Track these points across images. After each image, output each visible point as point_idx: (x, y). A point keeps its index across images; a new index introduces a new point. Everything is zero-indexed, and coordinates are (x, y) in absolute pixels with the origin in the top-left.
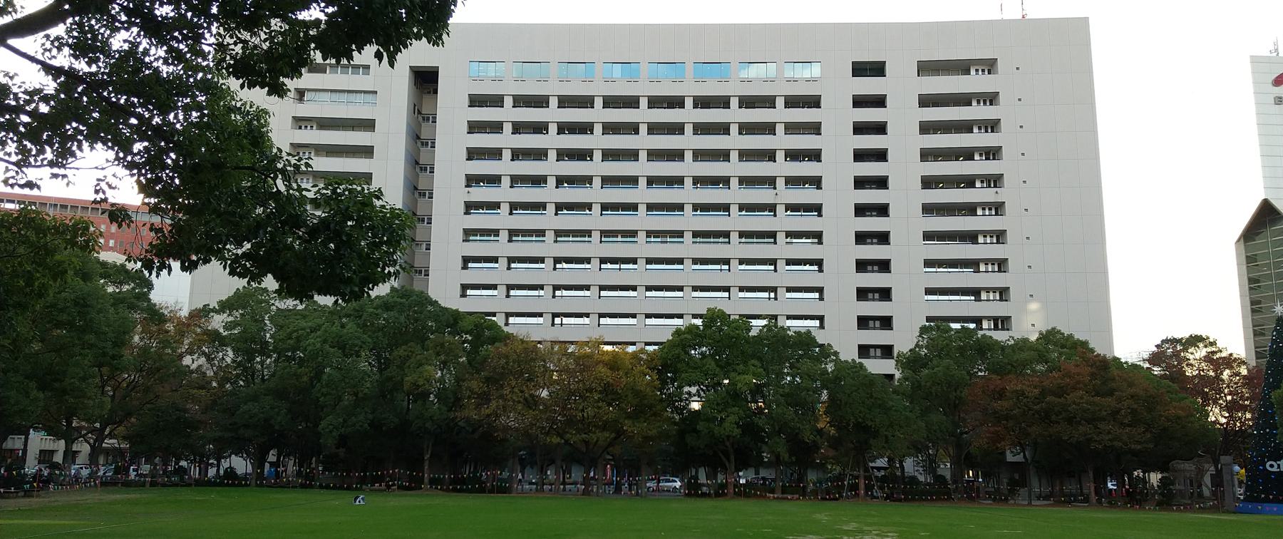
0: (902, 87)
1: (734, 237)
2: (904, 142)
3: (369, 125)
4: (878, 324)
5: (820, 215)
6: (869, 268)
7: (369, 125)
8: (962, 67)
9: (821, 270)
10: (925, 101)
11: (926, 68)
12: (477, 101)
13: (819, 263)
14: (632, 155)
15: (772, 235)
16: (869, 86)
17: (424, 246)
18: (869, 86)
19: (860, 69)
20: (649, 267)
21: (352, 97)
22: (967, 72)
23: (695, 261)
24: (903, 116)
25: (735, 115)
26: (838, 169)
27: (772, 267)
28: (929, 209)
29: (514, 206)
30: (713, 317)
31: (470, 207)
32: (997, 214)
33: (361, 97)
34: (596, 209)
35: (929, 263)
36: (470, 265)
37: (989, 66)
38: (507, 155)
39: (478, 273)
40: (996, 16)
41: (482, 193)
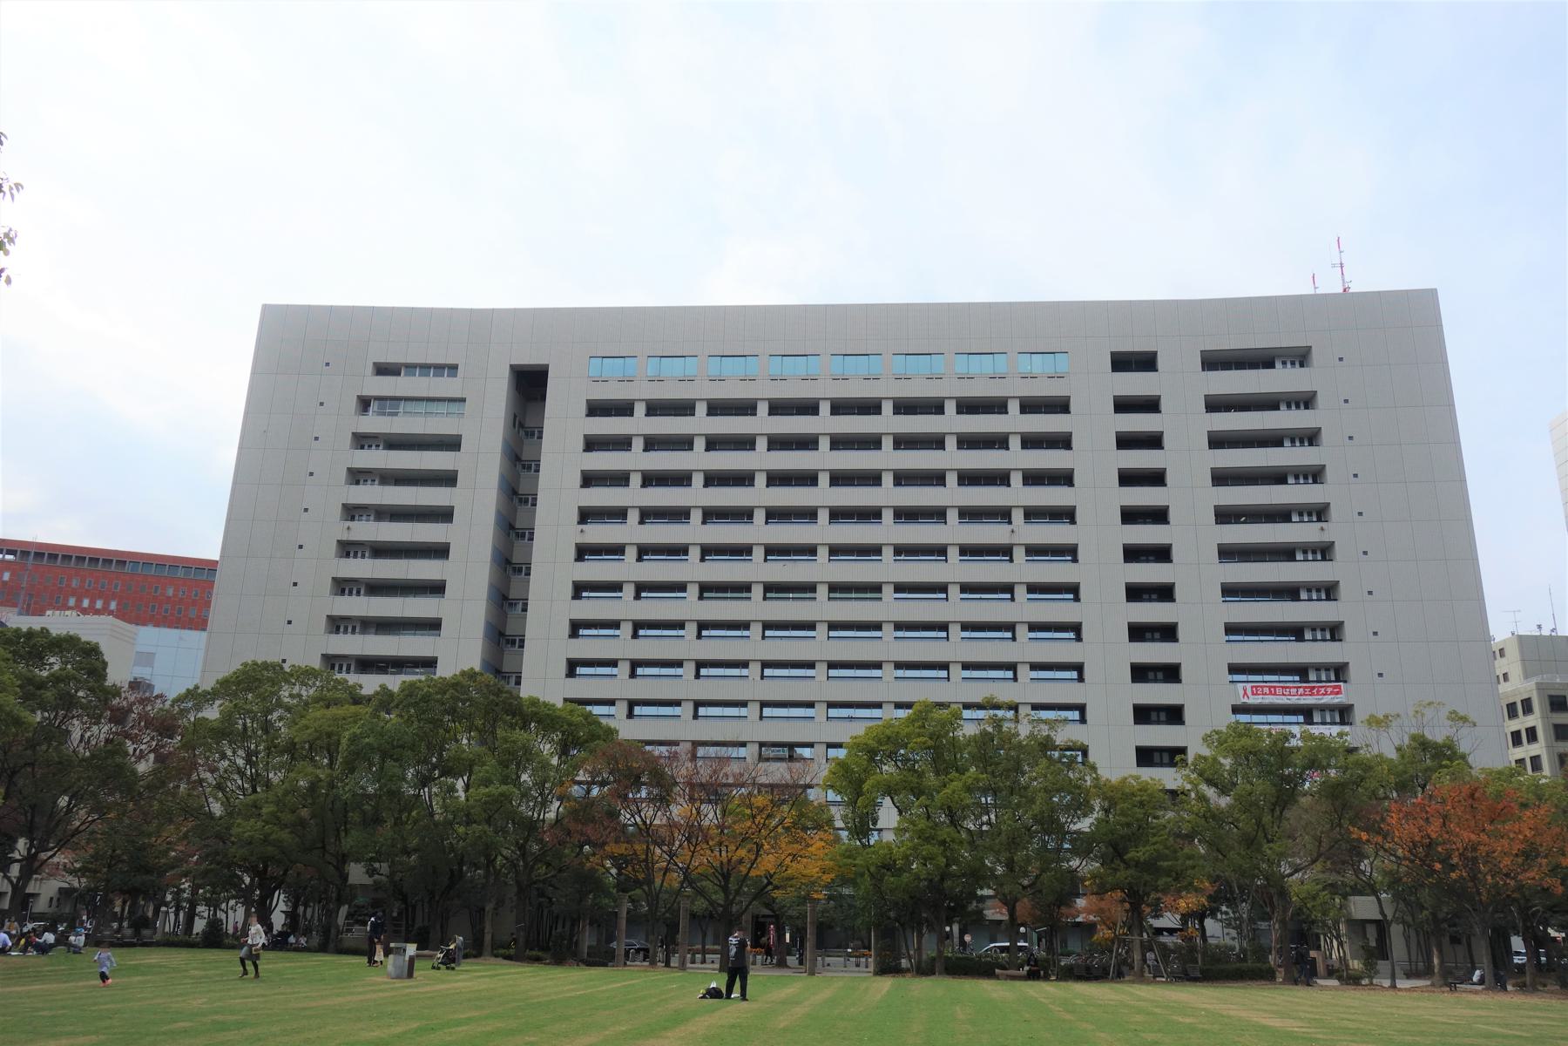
0: (1181, 387)
1: (953, 553)
2: (1187, 459)
3: (451, 444)
4: (1163, 716)
5: (1075, 560)
6: (1148, 635)
7: (451, 444)
8: (1263, 360)
9: (1081, 679)
10: (1215, 405)
11: (1214, 362)
12: (597, 409)
13: (1076, 629)
14: (808, 479)
15: (1008, 588)
16: (1136, 384)
17: (520, 606)
18: (1136, 384)
19: (1123, 362)
20: (832, 634)
21: (433, 407)
22: (1281, 445)
23: (899, 665)
24: (1185, 429)
25: (951, 423)
26: (1097, 496)
27: (1009, 635)
28: (1228, 553)
29: (641, 588)
30: (924, 712)
31: (583, 552)
32: (1324, 559)
33: (443, 408)
34: (758, 553)
35: (1231, 629)
36: (582, 632)
37: (1301, 357)
38: (638, 444)
39: (590, 646)
40: (1307, 290)
41: (598, 533)
